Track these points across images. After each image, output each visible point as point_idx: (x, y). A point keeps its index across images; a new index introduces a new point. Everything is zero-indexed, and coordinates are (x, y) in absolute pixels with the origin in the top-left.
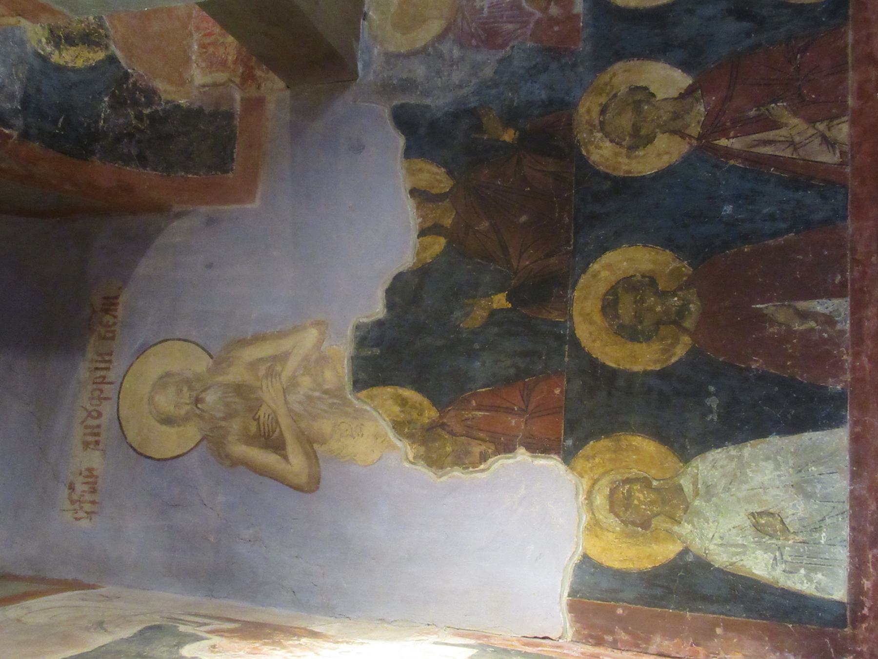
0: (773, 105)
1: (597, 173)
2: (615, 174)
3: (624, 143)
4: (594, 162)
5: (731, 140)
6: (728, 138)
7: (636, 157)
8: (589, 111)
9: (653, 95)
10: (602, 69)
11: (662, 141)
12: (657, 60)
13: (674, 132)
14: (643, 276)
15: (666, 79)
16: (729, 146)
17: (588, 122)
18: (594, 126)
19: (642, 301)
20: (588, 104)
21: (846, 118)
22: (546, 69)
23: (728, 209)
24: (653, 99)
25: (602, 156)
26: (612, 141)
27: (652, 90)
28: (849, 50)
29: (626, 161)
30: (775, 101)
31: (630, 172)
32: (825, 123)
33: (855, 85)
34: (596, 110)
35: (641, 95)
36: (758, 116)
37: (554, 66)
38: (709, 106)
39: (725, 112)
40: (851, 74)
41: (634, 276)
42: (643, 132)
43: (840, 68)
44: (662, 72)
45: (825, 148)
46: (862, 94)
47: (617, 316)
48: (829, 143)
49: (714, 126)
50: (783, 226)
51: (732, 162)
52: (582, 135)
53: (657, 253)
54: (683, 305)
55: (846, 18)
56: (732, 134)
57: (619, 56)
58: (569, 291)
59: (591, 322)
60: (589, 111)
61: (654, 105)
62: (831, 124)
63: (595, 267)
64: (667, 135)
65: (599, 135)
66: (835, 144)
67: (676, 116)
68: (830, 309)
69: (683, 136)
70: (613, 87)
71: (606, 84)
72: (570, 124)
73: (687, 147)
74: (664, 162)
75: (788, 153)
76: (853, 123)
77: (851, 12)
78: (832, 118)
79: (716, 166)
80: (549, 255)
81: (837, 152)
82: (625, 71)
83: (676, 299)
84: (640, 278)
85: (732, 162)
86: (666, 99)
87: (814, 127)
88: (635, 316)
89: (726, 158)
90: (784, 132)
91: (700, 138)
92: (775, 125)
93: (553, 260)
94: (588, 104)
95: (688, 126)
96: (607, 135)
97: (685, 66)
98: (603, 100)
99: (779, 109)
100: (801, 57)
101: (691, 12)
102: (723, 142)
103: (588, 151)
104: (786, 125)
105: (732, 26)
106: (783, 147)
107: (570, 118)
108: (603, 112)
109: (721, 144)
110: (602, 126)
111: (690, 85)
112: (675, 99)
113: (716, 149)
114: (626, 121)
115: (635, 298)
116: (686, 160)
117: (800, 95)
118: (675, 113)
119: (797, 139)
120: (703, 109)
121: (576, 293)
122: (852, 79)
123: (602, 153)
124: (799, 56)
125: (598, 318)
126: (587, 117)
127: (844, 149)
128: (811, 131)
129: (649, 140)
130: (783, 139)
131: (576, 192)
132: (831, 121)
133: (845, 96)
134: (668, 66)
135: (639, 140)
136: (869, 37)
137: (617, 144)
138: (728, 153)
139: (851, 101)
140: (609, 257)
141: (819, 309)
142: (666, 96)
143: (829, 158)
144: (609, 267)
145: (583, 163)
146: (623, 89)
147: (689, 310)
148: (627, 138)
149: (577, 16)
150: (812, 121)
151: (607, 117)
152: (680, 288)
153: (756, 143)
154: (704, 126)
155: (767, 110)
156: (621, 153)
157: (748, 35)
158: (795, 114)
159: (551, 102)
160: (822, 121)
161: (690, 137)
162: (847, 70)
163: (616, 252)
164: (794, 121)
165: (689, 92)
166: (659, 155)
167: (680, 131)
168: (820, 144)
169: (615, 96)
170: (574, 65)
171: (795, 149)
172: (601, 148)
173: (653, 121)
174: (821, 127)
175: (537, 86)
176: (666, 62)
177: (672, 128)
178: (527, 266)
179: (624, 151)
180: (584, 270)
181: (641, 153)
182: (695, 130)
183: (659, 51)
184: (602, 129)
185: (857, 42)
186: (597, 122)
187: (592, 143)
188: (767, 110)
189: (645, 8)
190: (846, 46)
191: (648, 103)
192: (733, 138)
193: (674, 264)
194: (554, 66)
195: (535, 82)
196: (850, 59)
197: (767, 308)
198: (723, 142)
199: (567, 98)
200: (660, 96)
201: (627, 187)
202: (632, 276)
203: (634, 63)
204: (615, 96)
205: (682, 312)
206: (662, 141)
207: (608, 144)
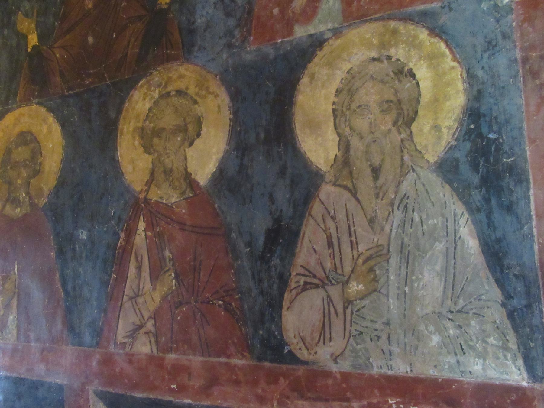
0: (173, 275)
1: (123, 102)
2: (121, 120)
3: (147, 122)
4: (132, 95)
5: (143, 234)
6: (145, 230)
7: (134, 138)
8: (181, 77)
9: (191, 144)
10: (224, 82)
11: (145, 162)
12: (230, 140)
13: (152, 173)
14: (41, 164)
15: (206, 156)
16: (138, 232)
17: (170, 78)
18: (166, 86)
19: (25, 166)
20: (188, 74)
21: (155, 351)
22: (228, 15)
23: (84, 235)
24: (186, 144)
25: (137, 102)
26: (150, 109)
27: (197, 142)
28: (223, 360)
29: (131, 129)
30: (177, 277)
31: (122, 134)
32: (153, 329)
33: (186, 363)
34: (181, 85)
35: (190, 131)
36: (164, 259)
37: (232, 22)
38: (177, 207)
39: (169, 224)
40: (200, 359)
41: (41, 156)
42: (156, 140)
43: (208, 348)
44: (214, 150)
45: (131, 328)
46: (178, 370)
47: (16, 147)
48: (133, 335)
49: (156, 213)
50: (69, 287)
51: (122, 235)
52: (156, 77)
53: (55, 173)
54: (19, 202)
55: (260, 359)
56: (149, 234)
57: (235, 96)
58: (37, 100)
59: (15, 125)
60: (181, 77)
61: (180, 147)
62: (151, 335)
63: (51, 119)
64: (151, 166)
65: (156, 95)
66: (133, 338)
67: (168, 173)
68: (10, 327)
69: (149, 183)
70: (204, 97)
71: (207, 89)
72: (169, 59)
73: (138, 189)
74: (127, 168)
75: (128, 291)
76: (151, 358)
77: (267, 364)
78: (156, 336)
79: (120, 219)
80: (62, 75)
81: (126, 340)
82: (219, 107)
83: (24, 195)
84: (39, 161)
85: (122, 235)
86: (186, 159)
87: (150, 317)
88: (16, 162)
89: (126, 229)
90: (148, 286)
91: (147, 201)
92: (155, 276)
93: (58, 79)
94: (188, 74)
95: (158, 187)
96: (156, 103)
97: (220, 175)
98: (192, 90)
99: (169, 281)
100: (220, 306)
101: (282, 173)
102: (142, 225)
103: (142, 86)
104: (154, 289)
105: (261, 224)
106: (134, 287)
107: (176, 58)
108: (180, 93)
109: (140, 224)
110: (166, 96)
111: (198, 183)
112: (186, 169)
113: (135, 219)
114: (169, 120)
115: (28, 160)
116: (128, 189)
117: (181, 304)
118: (171, 171)
119: (140, 300)
120: (173, 200)
121: (34, 107)
122: (196, 360)
123: (140, 102)
124: (221, 302)
125: (17, 130)
126: (175, 77)
127: (127, 346)
128: (146, 315)
129: (148, 149)
130: (141, 287)
131: (108, 85)
132: (154, 336)
133: (176, 350)
134: (221, 155)
135: (148, 138)
136: (237, 383)
137: (147, 116)
138: (131, 233)
139: (172, 356)
140: (56, 128)
141: (11, 317)
142: (189, 159)
143: (122, 331)
144: (50, 131)
145: (131, 84)
146: (199, 109)
147: (17, 207)
148: (152, 125)
149: (290, 32)
150: (156, 316)
151: (174, 99)
152: (31, 198)
153: (139, 259)
154: (157, 203)
155: (169, 269)
156: (139, 122)
157: (249, 244)
158: (164, 299)
159: (192, 32)
160: (155, 326)
161: (148, 191)
162: (203, 356)
163: (60, 135)
164: (157, 296)
165: (192, 183)
166: (133, 161)
167: (153, 180)
168: (133, 323)
169: (195, 102)
170: (230, 46)
171: (131, 298)
172: (144, 99)
173: (165, 149)
174: (150, 325)
175: (210, 11)
176: (226, 152)
177: (156, 169)
178: (56, 56)
179: (140, 125)
180: (51, 110)
181: (137, 143)
182: (154, 196)
183: (239, 146)
184: (162, 96)
185: (230, 368)
186: (170, 88)
187: (149, 89)
188: (169, 269)
189: (293, 114)
190: (229, 357)
191: (184, 140)
192: (146, 235)
193: (46, 190)
194: (232, 22)
195: (215, 7)
196: (214, 359)
197: (15, 274)
198: (142, 225)
199: (196, 48)
200: (190, 153)
201: (107, 135)
202: (41, 153)
203: (227, 115)
204: (195, 102)
205: (15, 201)
206: (145, 162)
207: (148, 106)
